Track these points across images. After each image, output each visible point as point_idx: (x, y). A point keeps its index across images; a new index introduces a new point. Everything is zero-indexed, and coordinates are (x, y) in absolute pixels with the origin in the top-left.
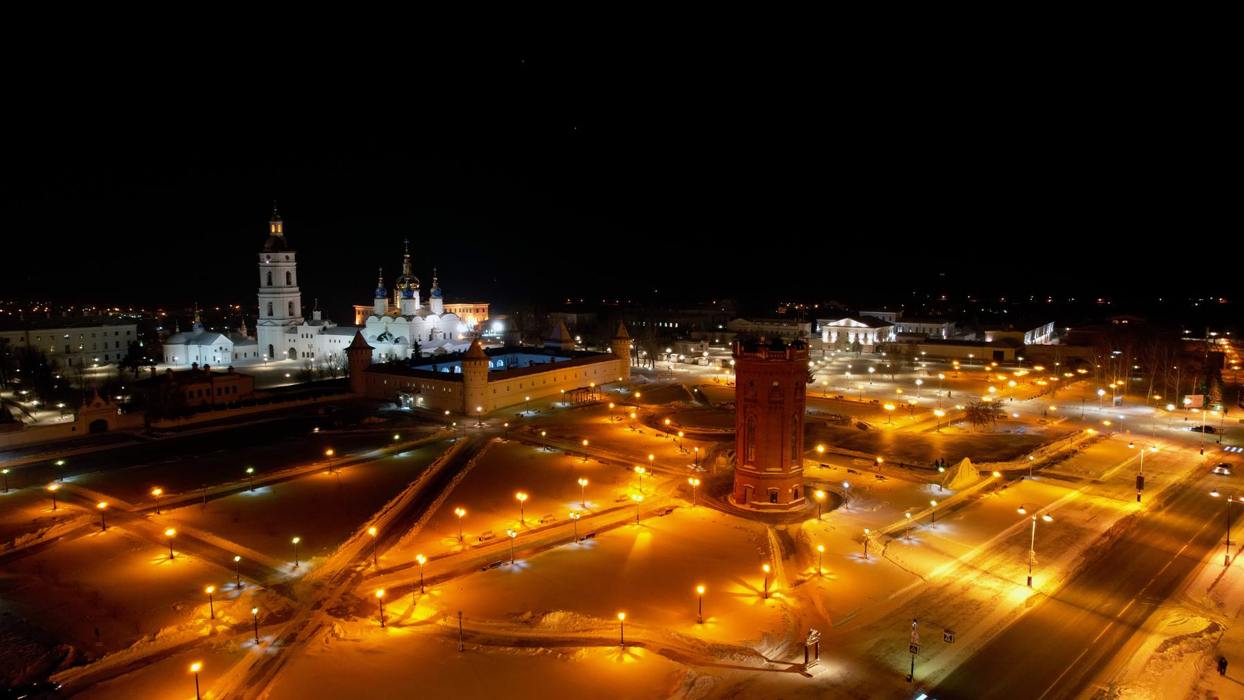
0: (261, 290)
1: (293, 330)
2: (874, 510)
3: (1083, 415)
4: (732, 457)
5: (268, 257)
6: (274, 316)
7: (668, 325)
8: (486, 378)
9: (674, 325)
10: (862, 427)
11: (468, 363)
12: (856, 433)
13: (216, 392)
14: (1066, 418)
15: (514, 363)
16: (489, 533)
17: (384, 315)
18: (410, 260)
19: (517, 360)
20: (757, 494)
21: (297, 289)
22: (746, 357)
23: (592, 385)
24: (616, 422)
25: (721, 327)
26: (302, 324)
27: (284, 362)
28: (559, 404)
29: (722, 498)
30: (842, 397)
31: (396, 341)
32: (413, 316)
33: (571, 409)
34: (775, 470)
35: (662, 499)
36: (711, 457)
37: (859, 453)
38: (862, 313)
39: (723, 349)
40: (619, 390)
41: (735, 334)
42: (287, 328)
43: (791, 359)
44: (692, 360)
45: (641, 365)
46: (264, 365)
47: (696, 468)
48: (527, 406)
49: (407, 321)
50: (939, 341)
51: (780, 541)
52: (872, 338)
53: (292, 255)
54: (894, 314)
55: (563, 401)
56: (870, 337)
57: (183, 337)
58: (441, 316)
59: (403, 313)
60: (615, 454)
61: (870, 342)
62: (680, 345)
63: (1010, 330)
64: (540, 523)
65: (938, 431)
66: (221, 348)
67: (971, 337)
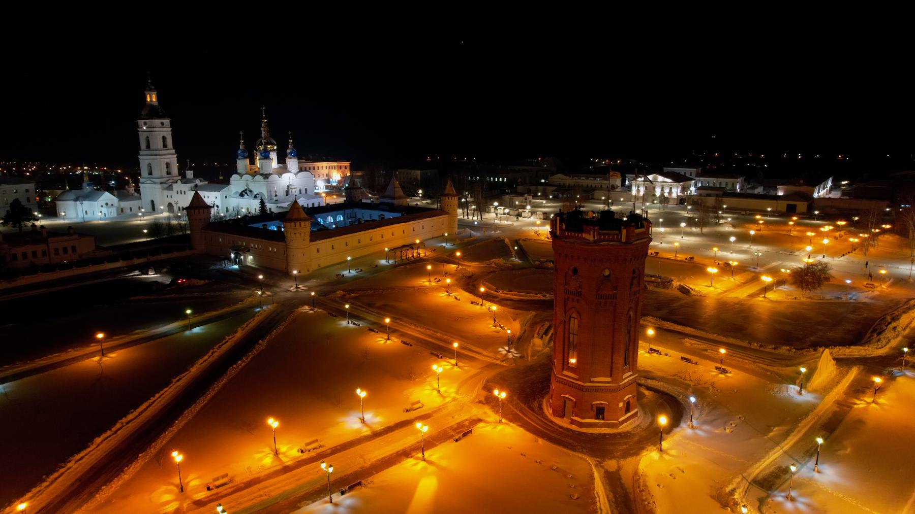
0: (141, 153)
1: (170, 188)
2: (728, 431)
3: (910, 276)
4: (550, 335)
5: (145, 124)
6: (153, 176)
7: (498, 179)
8: (308, 238)
9: (503, 180)
10: (685, 291)
11: (288, 224)
12: (678, 299)
13: (52, 252)
14: (891, 280)
15: (353, 217)
16: (223, 477)
17: (246, 174)
18: (268, 124)
19: (356, 215)
20: (580, 409)
21: (174, 151)
22: (568, 237)
23: (418, 241)
24: (433, 284)
25: (543, 181)
26: (176, 182)
27: (161, 215)
28: (383, 262)
29: (536, 404)
30: (658, 253)
31: (256, 197)
32: (270, 174)
33: (394, 266)
34: (602, 380)
35: (462, 408)
36: (526, 335)
37: (688, 330)
38: (666, 169)
39: (544, 202)
40: (444, 244)
41: (554, 188)
42: (164, 186)
43: (628, 242)
44: (516, 212)
45: (470, 217)
46: (139, 219)
47: (508, 352)
48: (349, 265)
49: (264, 179)
50: (734, 195)
51: (611, 496)
52: (676, 192)
53: (167, 122)
54: (694, 170)
55: (387, 259)
56: (674, 191)
57: (72, 195)
58: (296, 174)
59: (261, 172)
60: (422, 330)
61: (674, 195)
62: (506, 198)
63: (800, 185)
64: (300, 454)
65: (764, 297)
66: (107, 204)
67: (760, 190)
